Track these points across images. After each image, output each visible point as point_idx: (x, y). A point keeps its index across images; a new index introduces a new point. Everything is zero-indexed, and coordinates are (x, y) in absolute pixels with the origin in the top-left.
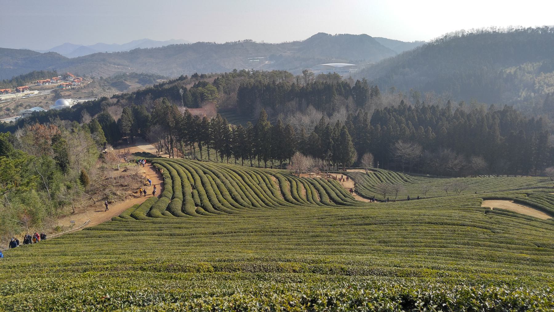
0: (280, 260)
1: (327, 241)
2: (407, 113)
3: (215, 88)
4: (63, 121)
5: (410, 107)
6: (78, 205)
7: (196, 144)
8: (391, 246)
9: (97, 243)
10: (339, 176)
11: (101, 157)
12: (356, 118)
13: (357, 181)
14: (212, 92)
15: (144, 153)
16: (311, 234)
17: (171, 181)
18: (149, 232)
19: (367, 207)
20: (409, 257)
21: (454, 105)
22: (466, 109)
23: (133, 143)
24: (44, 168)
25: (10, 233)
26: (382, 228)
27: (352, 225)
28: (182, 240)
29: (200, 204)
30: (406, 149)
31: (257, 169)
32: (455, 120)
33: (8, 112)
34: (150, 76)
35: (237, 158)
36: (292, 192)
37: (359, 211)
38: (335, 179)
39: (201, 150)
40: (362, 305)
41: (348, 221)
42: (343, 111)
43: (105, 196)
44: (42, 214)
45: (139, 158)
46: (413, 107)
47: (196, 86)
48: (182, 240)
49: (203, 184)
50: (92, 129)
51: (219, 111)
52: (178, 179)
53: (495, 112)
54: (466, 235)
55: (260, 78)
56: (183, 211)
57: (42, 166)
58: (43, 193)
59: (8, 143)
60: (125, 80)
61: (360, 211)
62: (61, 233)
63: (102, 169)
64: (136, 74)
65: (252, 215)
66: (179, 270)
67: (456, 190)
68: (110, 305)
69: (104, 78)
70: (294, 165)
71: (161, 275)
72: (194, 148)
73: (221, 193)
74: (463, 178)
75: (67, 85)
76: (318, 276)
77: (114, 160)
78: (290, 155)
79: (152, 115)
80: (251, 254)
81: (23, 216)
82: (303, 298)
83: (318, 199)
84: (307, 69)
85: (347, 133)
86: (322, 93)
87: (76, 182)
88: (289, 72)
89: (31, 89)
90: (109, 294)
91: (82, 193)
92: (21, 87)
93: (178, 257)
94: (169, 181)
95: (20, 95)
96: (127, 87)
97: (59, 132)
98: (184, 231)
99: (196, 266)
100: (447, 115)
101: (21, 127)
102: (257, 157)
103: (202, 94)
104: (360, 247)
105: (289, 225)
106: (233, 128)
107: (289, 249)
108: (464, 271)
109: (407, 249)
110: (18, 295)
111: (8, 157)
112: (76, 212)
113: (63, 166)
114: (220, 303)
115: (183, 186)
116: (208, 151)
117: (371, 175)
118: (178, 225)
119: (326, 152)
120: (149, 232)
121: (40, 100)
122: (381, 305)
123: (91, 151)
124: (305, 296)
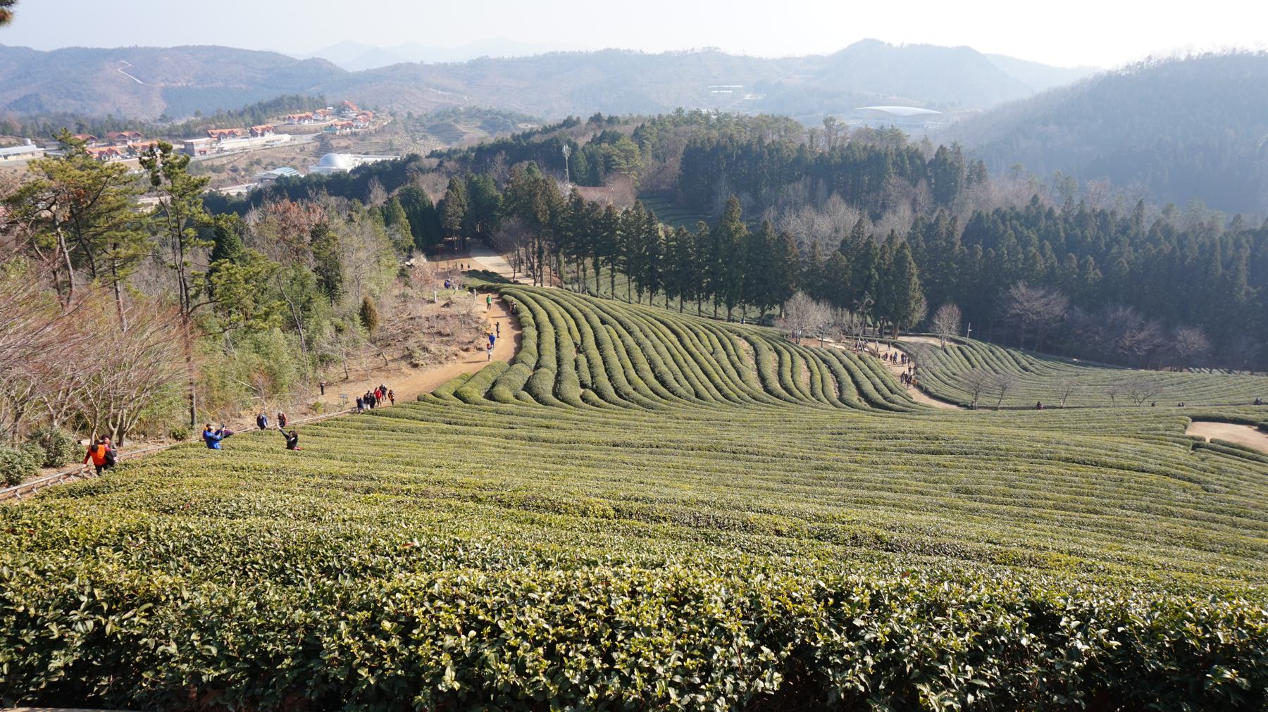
0: (749, 508)
1: (847, 480)
2: (1043, 223)
3: (634, 147)
4: (333, 198)
5: (1051, 210)
6: (354, 364)
7: (589, 262)
8: (981, 500)
9: (388, 442)
10: (883, 349)
11: (402, 274)
12: (930, 227)
13: (920, 362)
14: (628, 155)
15: (485, 272)
16: (814, 463)
17: (535, 333)
18: (489, 430)
19: (936, 417)
20: (1019, 526)
21: (1152, 212)
22: (1178, 223)
24: (296, 287)
25: (234, 406)
26: (965, 461)
27: (900, 451)
28: (552, 452)
29: (589, 383)
30: (1029, 301)
31: (710, 321)
32: (1149, 245)
33: (234, 175)
34: (505, 116)
35: (670, 294)
36: (780, 375)
37: (920, 425)
38: (874, 354)
39: (598, 273)
40: (945, 615)
41: (894, 442)
42: (905, 211)
43: (406, 353)
45: (478, 283)
46: (1058, 212)
47: (597, 141)
48: (552, 452)
51: (641, 196)
53: (1243, 233)
54: (1145, 492)
55: (732, 130)
56: (556, 394)
57: (292, 284)
58: (291, 336)
59: (232, 235)
60: (456, 121)
61: (920, 423)
62: (323, 416)
63: (404, 298)
64: (479, 111)
65: (694, 416)
66: (546, 508)
67: (1134, 396)
68: (420, 560)
69: (415, 115)
70: (789, 320)
71: (513, 514)
72: (584, 270)
73: (634, 365)
74: (1153, 372)
75: (342, 126)
76: (829, 547)
77: (427, 281)
78: (783, 296)
79: (505, 195)
80: (689, 493)
81: (256, 376)
82: (817, 587)
83: (834, 394)
84: (835, 116)
85: (910, 258)
86: (861, 169)
87: (352, 320)
88: (795, 119)
89: (277, 131)
90: (419, 540)
91: (363, 342)
92: (259, 127)
94: (531, 332)
95: (258, 141)
96: (459, 136)
97: (326, 219)
98: (557, 435)
99: (581, 504)
100: (1132, 233)
101: (257, 206)
102: (712, 297)
103: (608, 158)
104: (914, 497)
105: (770, 442)
106: (666, 232)
107: (767, 489)
109: (1016, 510)
110: (251, 520)
111: (232, 261)
112: (351, 378)
113: (330, 285)
114: (645, 579)
115: (558, 345)
116: (613, 277)
117: (951, 352)
118: (545, 422)
119: (860, 296)
120: (489, 430)
121: (293, 154)
122: (984, 618)
123: (384, 260)
124: (823, 585)
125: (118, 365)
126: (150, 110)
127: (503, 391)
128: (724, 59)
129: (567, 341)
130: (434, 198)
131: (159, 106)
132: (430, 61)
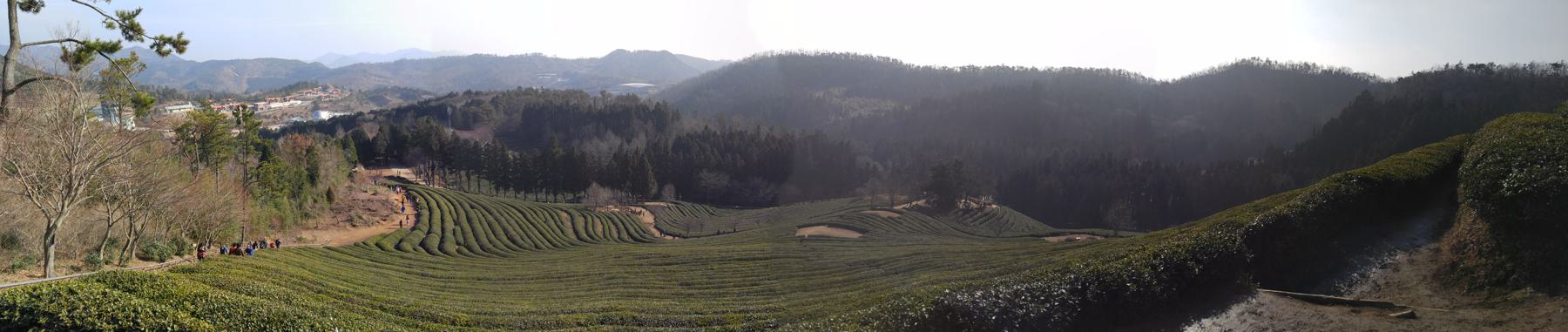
14: (488, 113)
21: (764, 130)
23: (388, 165)
30: (710, 179)
35: (517, 191)
37: (659, 249)
42: (642, 137)
44: (289, 221)
45: (394, 183)
47: (468, 105)
49: (469, 220)
50: (345, 145)
51: (496, 135)
52: (437, 213)
63: (350, 188)
86: (623, 115)
93: (429, 303)
98: (440, 273)
105: (581, 269)
108: (775, 310)
113: (313, 178)
125: (213, 209)
126: (240, 89)
127: (406, 245)
128: (545, 59)
129: (448, 218)
130: (370, 136)
131: (245, 87)
132: (373, 61)
